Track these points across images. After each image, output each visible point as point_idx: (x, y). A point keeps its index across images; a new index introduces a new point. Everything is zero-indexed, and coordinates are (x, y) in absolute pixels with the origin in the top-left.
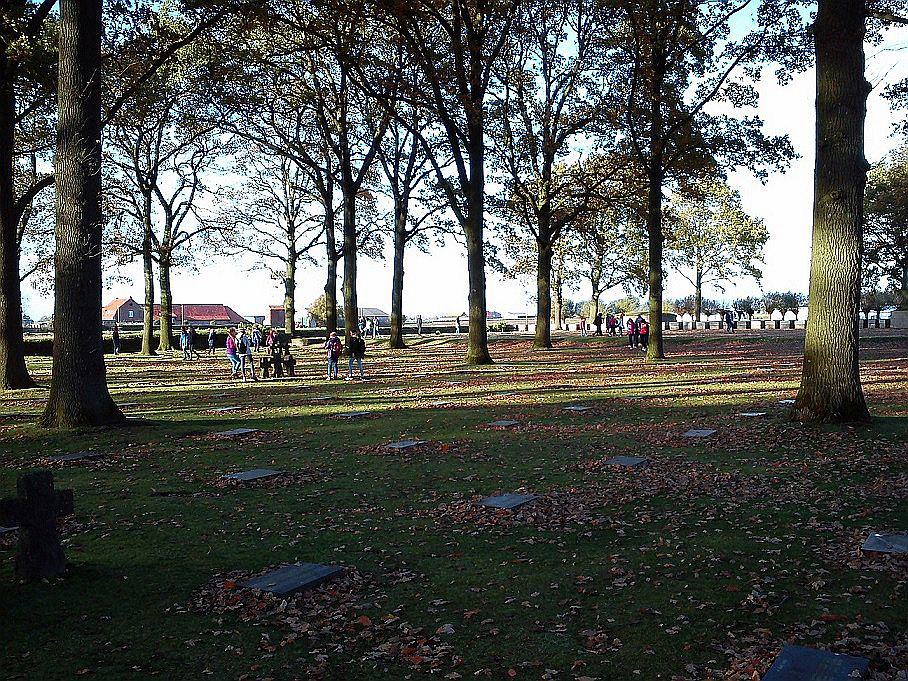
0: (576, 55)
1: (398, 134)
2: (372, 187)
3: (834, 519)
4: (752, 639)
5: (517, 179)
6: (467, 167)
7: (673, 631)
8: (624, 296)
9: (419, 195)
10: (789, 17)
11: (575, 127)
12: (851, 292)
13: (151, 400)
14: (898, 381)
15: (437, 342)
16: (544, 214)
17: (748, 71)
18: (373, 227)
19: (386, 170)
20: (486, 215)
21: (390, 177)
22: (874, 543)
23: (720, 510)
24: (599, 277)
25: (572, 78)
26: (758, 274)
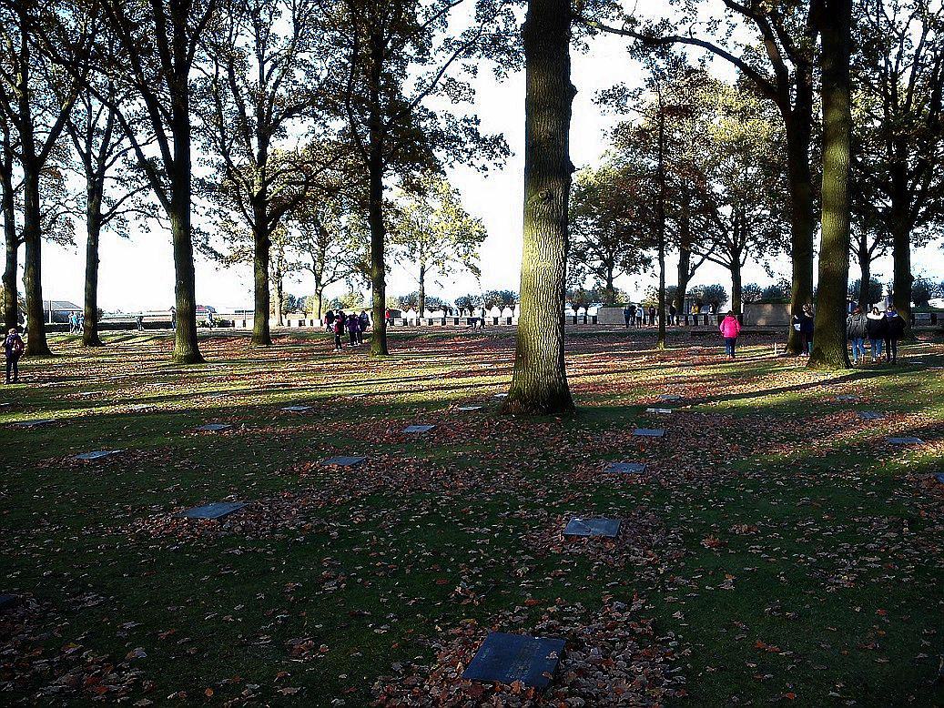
0: (291, 35)
1: (90, 106)
2: (60, 164)
3: (538, 506)
4: (459, 630)
5: (230, 163)
6: (171, 145)
7: (382, 630)
8: (347, 290)
9: (116, 174)
10: (504, 17)
11: (289, 114)
12: (557, 290)
13: (317, 351)
14: (603, 373)
15: (140, 339)
16: (258, 202)
17: (467, 68)
18: (62, 209)
19: (77, 145)
20: (193, 198)
21: (81, 153)
22: (575, 528)
23: (434, 504)
24: (322, 270)
25: (287, 62)
26: (476, 271)
